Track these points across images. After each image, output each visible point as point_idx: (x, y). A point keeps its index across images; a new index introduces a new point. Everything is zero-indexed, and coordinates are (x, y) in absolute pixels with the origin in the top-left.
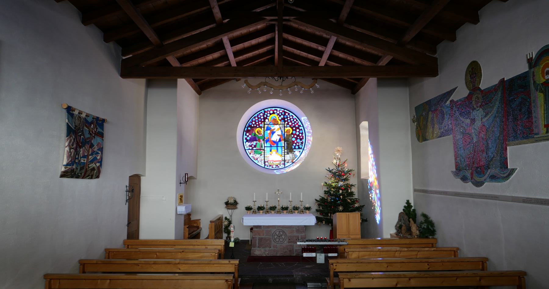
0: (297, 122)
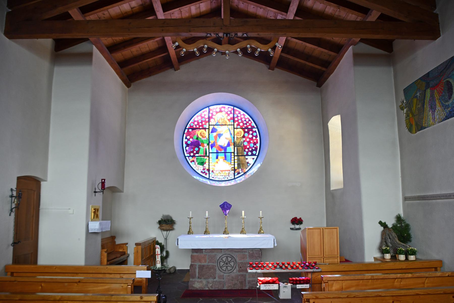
0: (250, 122)
